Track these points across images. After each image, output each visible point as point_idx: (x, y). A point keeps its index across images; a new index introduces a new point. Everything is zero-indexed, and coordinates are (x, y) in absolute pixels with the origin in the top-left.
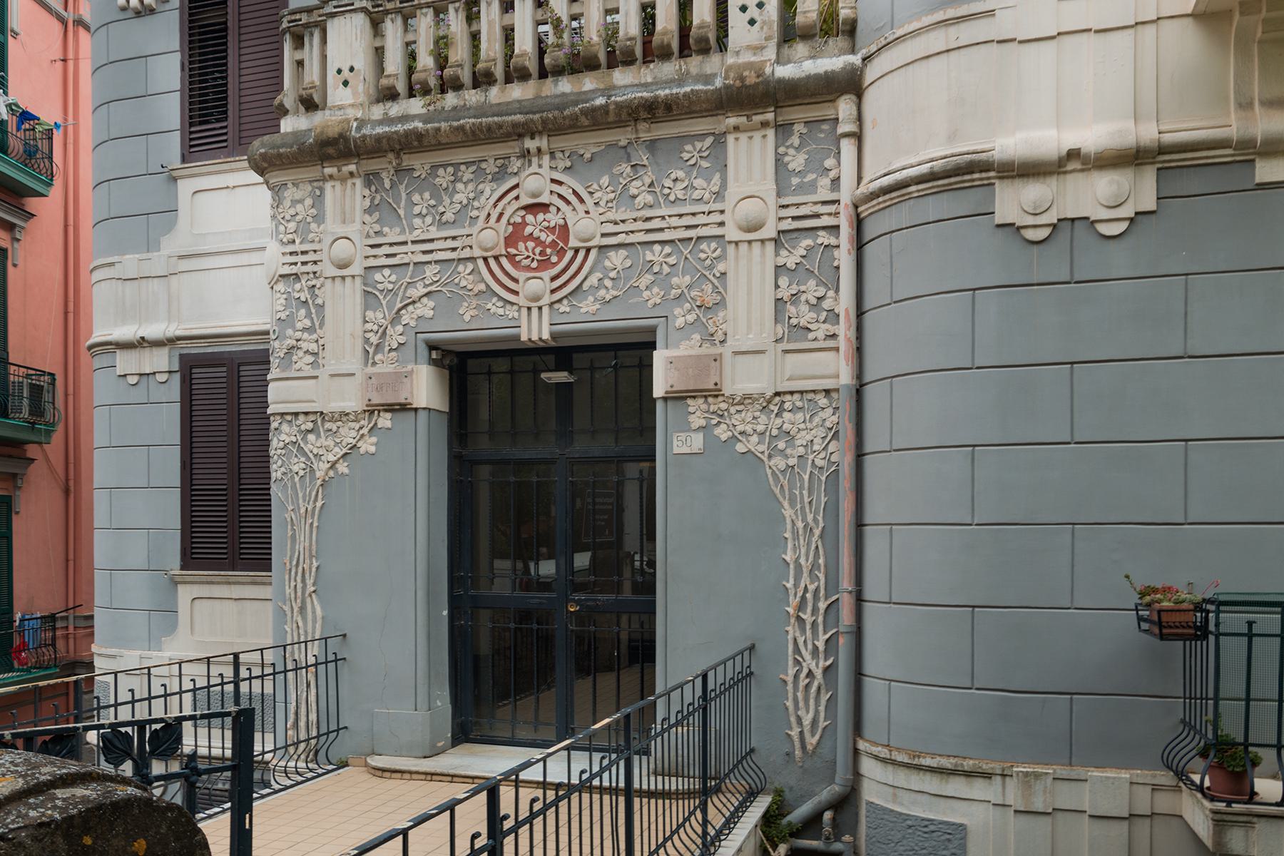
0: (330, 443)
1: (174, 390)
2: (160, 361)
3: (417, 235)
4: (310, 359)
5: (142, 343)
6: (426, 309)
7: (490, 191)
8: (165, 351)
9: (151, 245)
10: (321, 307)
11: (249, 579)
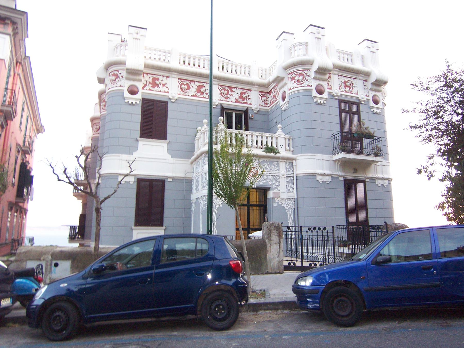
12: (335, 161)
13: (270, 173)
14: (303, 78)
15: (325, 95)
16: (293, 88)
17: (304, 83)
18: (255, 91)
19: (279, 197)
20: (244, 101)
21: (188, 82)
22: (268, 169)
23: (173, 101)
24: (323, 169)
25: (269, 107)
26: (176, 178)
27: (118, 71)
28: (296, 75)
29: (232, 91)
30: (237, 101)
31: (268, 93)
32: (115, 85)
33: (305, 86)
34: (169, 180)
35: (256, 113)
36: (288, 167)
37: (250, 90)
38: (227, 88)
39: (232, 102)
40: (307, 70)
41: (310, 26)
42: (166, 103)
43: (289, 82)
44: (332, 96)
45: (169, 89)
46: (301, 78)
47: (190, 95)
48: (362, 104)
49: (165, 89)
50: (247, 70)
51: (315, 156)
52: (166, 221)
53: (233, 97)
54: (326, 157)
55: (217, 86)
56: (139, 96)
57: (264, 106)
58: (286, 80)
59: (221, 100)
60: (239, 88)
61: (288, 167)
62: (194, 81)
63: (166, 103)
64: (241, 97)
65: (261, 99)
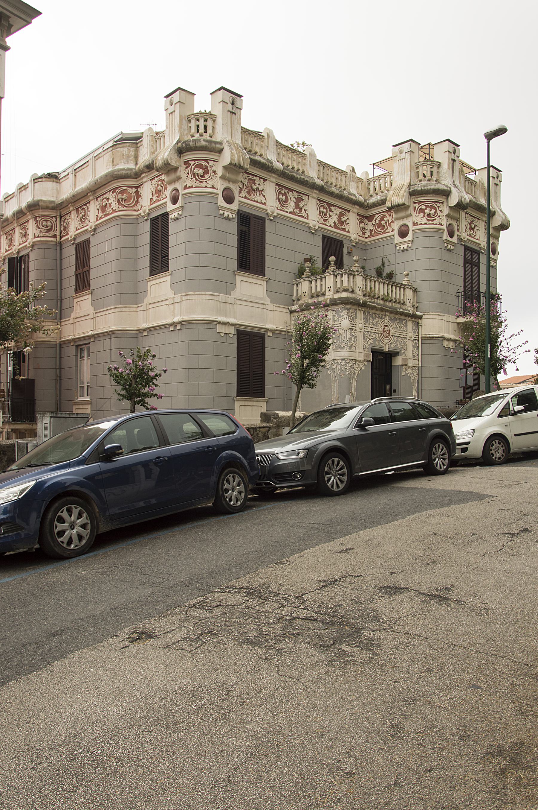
0: (358, 366)
1: (235, 340)
2: (231, 331)
3: (371, 326)
4: (354, 348)
5: (228, 324)
6: (371, 341)
7: (380, 321)
8: (233, 327)
9: (228, 293)
10: (356, 337)
11: (256, 400)
12: (458, 324)
13: (400, 333)
14: (435, 213)
15: (455, 240)
16: (421, 224)
17: (435, 219)
18: (354, 213)
19: (406, 365)
20: (342, 227)
21: (286, 191)
22: (398, 329)
23: (272, 218)
24: (449, 333)
25: (366, 238)
26: (276, 332)
27: (206, 161)
28: (427, 206)
29: (331, 211)
30: (335, 227)
31: (366, 218)
32: (204, 184)
33: (436, 224)
34: (269, 334)
35: (354, 246)
36: (414, 328)
37: (349, 211)
38: (326, 206)
39: (330, 226)
40: (440, 203)
41: (447, 142)
42: (263, 220)
43: (414, 214)
44: (460, 240)
45: (266, 199)
46: (433, 212)
47: (289, 211)
48: (482, 253)
49: (259, 198)
50: (202, 124)
51: (443, 316)
52: (268, 391)
53: (331, 220)
54: (452, 318)
55: (316, 200)
56: (235, 206)
57: (362, 237)
58: (411, 211)
59: (194, 186)
60: (337, 207)
61: (414, 328)
62: (292, 190)
63: (263, 220)
64: (340, 220)
65: (359, 225)
